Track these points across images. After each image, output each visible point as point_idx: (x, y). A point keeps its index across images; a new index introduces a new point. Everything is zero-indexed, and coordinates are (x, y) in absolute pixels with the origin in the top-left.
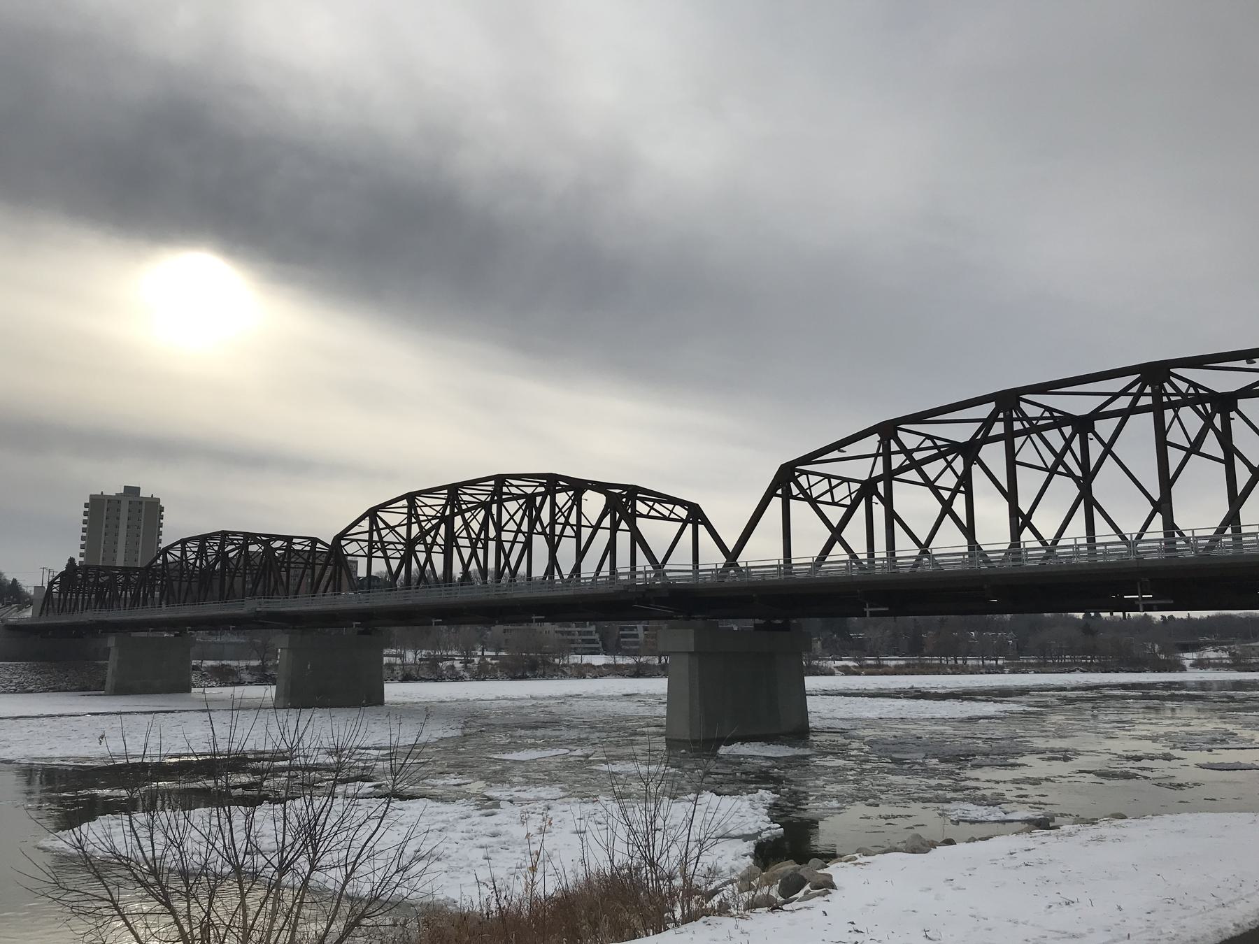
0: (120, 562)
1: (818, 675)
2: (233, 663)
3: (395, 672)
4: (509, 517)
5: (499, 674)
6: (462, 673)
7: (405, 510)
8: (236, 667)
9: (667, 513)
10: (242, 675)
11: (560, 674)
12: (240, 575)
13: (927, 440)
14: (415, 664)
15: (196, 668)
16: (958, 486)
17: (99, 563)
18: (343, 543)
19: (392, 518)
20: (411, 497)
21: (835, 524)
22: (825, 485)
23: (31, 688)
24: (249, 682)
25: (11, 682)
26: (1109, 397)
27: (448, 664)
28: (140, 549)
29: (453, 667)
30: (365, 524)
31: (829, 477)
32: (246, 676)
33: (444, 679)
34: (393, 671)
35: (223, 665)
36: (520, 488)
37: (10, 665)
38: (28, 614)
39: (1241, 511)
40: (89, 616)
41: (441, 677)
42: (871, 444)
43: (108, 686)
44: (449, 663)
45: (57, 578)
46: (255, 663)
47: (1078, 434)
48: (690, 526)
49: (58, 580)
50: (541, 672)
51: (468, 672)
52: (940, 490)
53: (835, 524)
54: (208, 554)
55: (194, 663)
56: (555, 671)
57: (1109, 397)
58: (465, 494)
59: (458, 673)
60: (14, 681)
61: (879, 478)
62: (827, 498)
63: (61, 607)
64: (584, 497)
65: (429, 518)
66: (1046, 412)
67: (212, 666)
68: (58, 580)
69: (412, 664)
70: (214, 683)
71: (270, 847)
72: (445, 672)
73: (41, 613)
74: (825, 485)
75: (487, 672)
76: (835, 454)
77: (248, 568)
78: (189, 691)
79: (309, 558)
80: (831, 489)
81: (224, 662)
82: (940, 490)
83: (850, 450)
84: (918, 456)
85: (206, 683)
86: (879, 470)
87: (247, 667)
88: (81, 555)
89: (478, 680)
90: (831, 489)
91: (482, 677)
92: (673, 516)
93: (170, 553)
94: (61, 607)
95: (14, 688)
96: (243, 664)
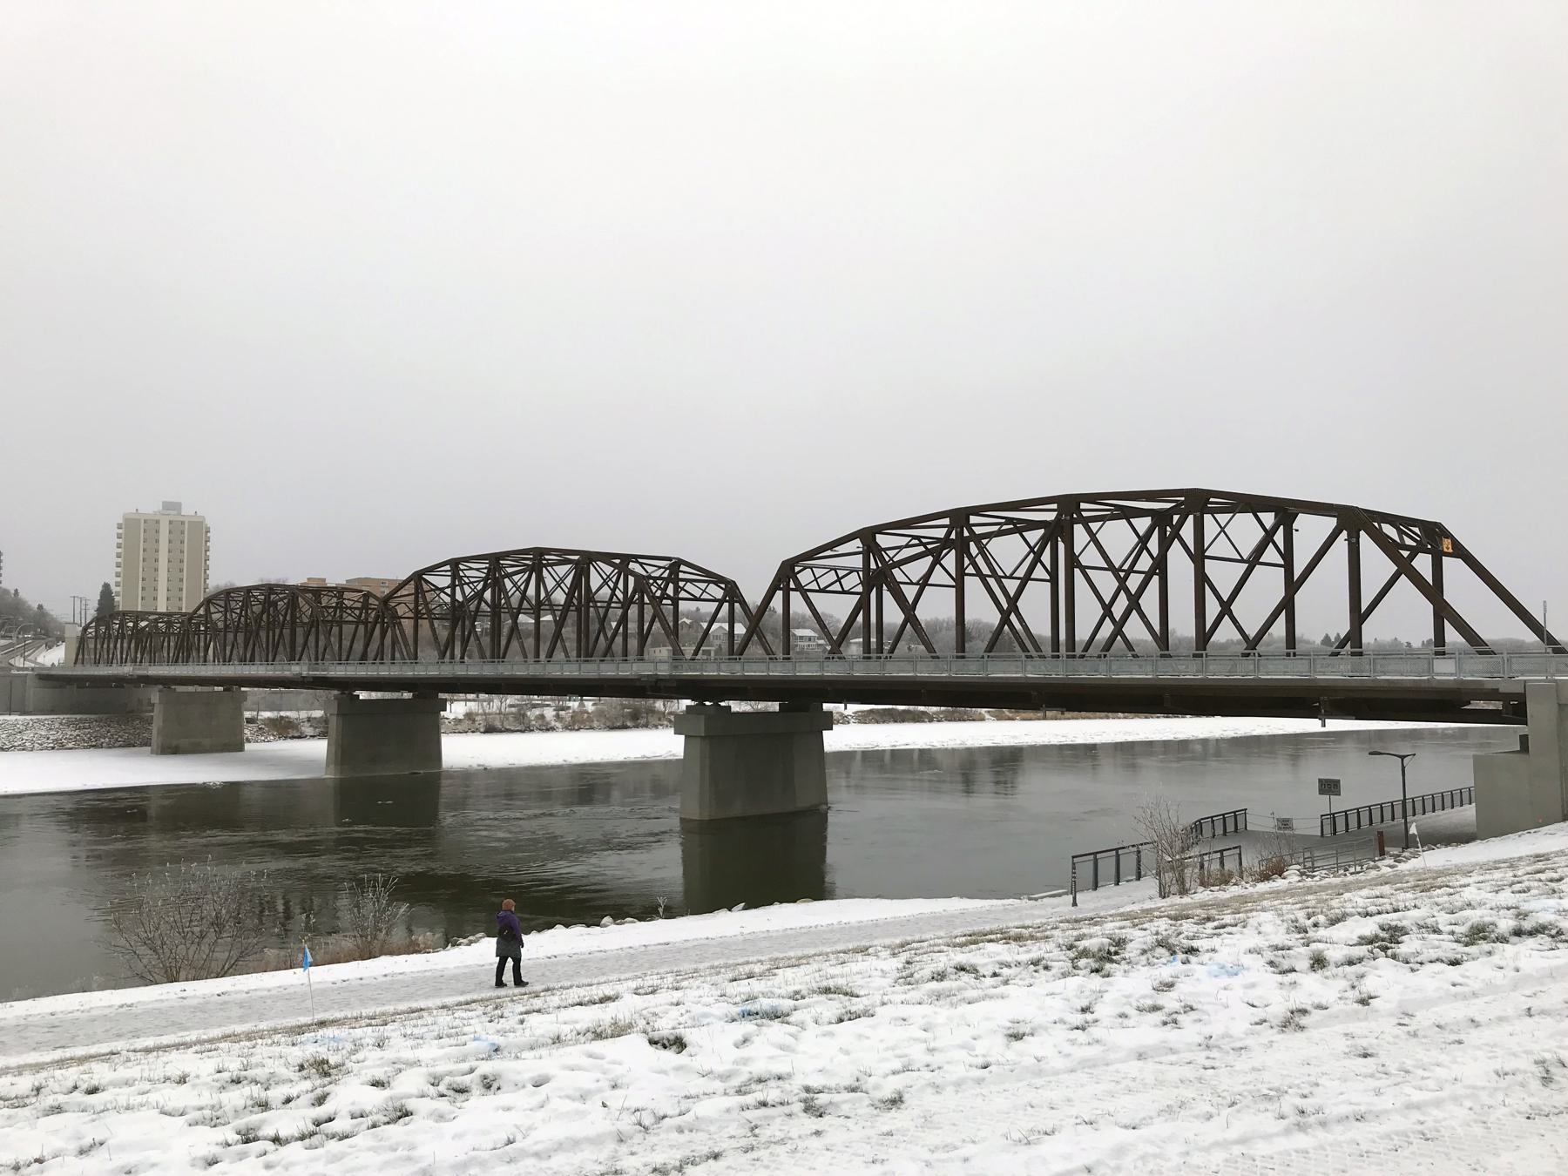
0: (162, 608)
1: (964, 720)
2: (292, 714)
3: (477, 723)
4: (1029, 549)
5: (595, 724)
6: (553, 723)
8: (296, 719)
9: (697, 593)
10: (303, 728)
11: (665, 723)
12: (574, 608)
14: (500, 713)
15: (250, 721)
16: (724, 596)
18: (797, 569)
19: (442, 581)
20: (455, 564)
22: (832, 576)
23: (70, 745)
24: (311, 736)
25: (48, 739)
27: (537, 713)
29: (542, 717)
30: (410, 588)
31: (835, 569)
32: (308, 730)
33: (533, 730)
34: (474, 721)
35: (281, 717)
37: (45, 720)
38: (54, 657)
39: (1296, 596)
40: (127, 670)
41: (529, 727)
42: (856, 545)
43: (859, 757)
44: (537, 712)
45: (91, 623)
46: (318, 714)
47: (1282, 527)
48: (726, 605)
49: (94, 624)
50: (642, 721)
51: (561, 722)
52: (1087, 570)
54: (681, 575)
55: (247, 714)
56: (660, 720)
58: (471, 569)
59: (548, 723)
60: (51, 737)
62: (814, 586)
63: (124, 656)
64: (1295, 526)
67: (269, 719)
68: (94, 624)
69: (496, 714)
70: (272, 738)
72: (534, 723)
73: (75, 663)
74: (832, 576)
75: (583, 722)
76: (829, 553)
77: (591, 604)
78: (242, 749)
79: (361, 614)
80: (839, 580)
81: (283, 714)
82: (1087, 570)
83: (841, 549)
84: (562, 585)
85: (263, 738)
87: (309, 719)
89: (571, 730)
90: (839, 580)
91: (576, 728)
92: (705, 596)
93: (212, 603)
94: (124, 656)
95: (52, 745)
96: (303, 715)
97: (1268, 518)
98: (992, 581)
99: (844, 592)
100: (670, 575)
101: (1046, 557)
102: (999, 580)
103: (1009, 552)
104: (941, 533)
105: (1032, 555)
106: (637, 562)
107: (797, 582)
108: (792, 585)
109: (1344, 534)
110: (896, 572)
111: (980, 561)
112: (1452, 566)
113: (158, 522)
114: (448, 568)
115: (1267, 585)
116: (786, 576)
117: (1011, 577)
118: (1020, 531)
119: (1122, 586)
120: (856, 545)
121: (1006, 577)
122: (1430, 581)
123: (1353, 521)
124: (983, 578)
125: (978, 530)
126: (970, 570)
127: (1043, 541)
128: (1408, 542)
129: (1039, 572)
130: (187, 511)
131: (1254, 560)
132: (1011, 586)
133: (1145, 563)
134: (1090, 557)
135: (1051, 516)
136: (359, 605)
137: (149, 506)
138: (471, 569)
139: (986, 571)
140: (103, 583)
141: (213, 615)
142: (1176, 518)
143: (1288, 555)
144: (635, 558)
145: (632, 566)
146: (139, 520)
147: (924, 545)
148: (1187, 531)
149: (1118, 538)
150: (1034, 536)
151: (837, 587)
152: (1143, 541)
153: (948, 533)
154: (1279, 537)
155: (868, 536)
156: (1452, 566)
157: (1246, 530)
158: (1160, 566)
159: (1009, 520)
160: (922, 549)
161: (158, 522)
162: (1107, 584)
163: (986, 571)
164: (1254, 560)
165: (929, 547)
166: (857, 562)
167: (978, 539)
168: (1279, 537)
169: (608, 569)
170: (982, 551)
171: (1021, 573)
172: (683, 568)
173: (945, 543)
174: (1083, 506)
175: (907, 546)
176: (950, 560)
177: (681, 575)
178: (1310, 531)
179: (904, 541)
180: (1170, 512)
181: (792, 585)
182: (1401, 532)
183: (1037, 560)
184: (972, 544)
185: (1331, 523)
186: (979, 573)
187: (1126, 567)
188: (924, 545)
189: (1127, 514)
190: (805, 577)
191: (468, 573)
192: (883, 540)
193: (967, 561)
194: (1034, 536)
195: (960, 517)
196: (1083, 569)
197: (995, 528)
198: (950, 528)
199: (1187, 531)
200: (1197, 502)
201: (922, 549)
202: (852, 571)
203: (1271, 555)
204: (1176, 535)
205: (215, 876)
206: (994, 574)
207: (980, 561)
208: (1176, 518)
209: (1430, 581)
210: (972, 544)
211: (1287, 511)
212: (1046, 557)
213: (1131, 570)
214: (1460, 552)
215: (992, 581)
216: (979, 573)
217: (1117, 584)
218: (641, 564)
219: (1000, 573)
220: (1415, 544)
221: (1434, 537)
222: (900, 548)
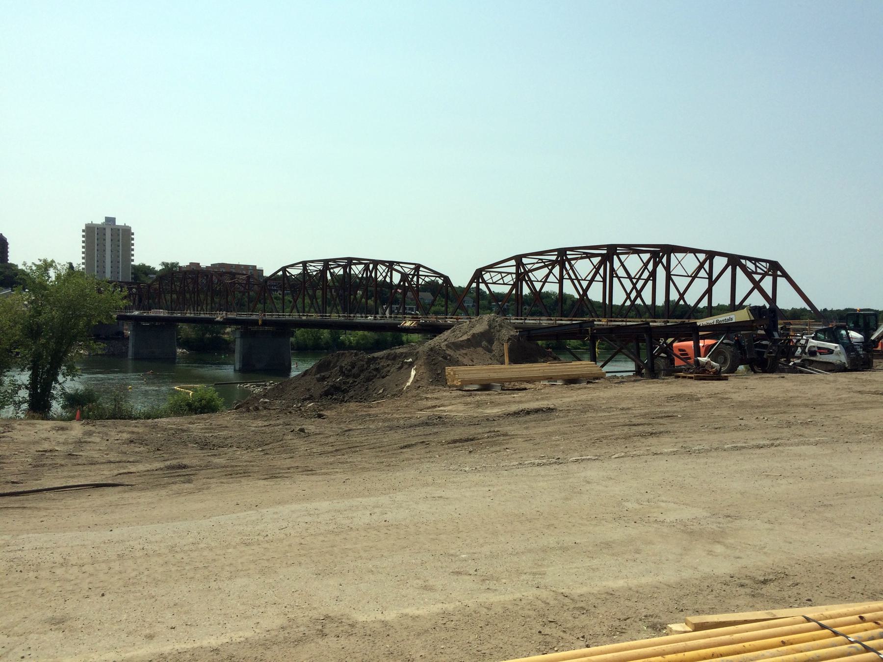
4: (752, 286)
7: (302, 268)
13: (400, 275)
17: (689, 347)
18: (483, 273)
21: (701, 261)
22: (499, 276)
26: (707, 297)
28: (120, 271)
31: (500, 273)
36: (707, 296)
42: (513, 262)
53: (701, 261)
57: (707, 296)
58: (311, 266)
61: (411, 275)
62: (490, 281)
65: (543, 280)
66: (399, 275)
71: (856, 375)
80: (502, 278)
86: (412, 273)
88: (83, 263)
90: (502, 278)
97: (702, 257)
98: (576, 282)
99: (504, 284)
100: (415, 272)
101: (601, 271)
102: (579, 281)
103: (584, 268)
104: (554, 258)
105: (595, 270)
106: (399, 266)
107: (483, 279)
108: (481, 281)
109: (730, 268)
110: (530, 274)
111: (571, 272)
112: (781, 281)
113: (104, 229)
114: (301, 265)
115: (701, 285)
116: (478, 275)
117: (585, 280)
118: (589, 258)
119: (634, 287)
120: (513, 262)
121: (582, 280)
122: (707, 295)
123: (734, 261)
124: (572, 280)
125: (569, 257)
126: (566, 276)
127: (601, 263)
128: (759, 271)
129: (598, 278)
130: (118, 223)
131: (694, 277)
132: (634, 281)
133: (646, 275)
134: (621, 272)
135: (605, 252)
136: (245, 282)
137: (99, 220)
138: (311, 266)
139: (573, 277)
140: (178, 261)
141: (515, 264)
142: (661, 254)
143: (710, 274)
144: (398, 263)
145: (397, 267)
146: (95, 227)
147: (544, 262)
148: (664, 260)
149: (634, 263)
150: (596, 260)
151: (501, 281)
152: (646, 265)
153: (557, 258)
154: (707, 266)
155: (518, 259)
156: (781, 281)
157: (690, 262)
158: (653, 275)
159: (584, 253)
160: (543, 264)
161: (104, 229)
162: (628, 285)
163: (573, 277)
164: (694, 277)
165: (546, 263)
166: (513, 270)
167: (569, 261)
168: (707, 266)
169: (384, 268)
170: (572, 267)
171: (589, 278)
172: (421, 269)
173: (553, 264)
174: (568, 252)
175: (537, 263)
176: (556, 271)
177: (421, 273)
178: (719, 263)
179: (536, 261)
180: (658, 252)
181: (481, 281)
182: (756, 267)
183: (597, 272)
184: (566, 263)
185: (725, 260)
186: (570, 278)
187: (637, 277)
188: (544, 262)
189: (589, 256)
190: (487, 277)
191: (311, 268)
192: (525, 261)
193: (565, 272)
194: (596, 260)
195: (562, 252)
196: (619, 278)
197: (580, 256)
198: (558, 256)
199: (664, 260)
200: (670, 250)
201: (543, 264)
202: (509, 273)
203: (702, 273)
204: (660, 261)
205: (290, 412)
206: (577, 279)
207: (571, 272)
208: (661, 254)
209: (707, 295)
210: (566, 263)
211: (711, 255)
212: (601, 271)
213: (639, 278)
214: (785, 275)
215: (576, 282)
216: (570, 278)
217: (632, 286)
218: (401, 267)
219: (580, 278)
220: (488, 292)
221: (775, 269)
222: (534, 264)
